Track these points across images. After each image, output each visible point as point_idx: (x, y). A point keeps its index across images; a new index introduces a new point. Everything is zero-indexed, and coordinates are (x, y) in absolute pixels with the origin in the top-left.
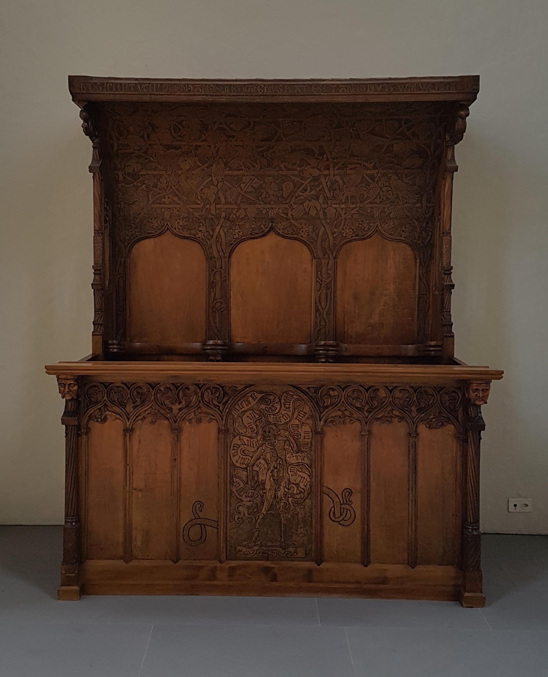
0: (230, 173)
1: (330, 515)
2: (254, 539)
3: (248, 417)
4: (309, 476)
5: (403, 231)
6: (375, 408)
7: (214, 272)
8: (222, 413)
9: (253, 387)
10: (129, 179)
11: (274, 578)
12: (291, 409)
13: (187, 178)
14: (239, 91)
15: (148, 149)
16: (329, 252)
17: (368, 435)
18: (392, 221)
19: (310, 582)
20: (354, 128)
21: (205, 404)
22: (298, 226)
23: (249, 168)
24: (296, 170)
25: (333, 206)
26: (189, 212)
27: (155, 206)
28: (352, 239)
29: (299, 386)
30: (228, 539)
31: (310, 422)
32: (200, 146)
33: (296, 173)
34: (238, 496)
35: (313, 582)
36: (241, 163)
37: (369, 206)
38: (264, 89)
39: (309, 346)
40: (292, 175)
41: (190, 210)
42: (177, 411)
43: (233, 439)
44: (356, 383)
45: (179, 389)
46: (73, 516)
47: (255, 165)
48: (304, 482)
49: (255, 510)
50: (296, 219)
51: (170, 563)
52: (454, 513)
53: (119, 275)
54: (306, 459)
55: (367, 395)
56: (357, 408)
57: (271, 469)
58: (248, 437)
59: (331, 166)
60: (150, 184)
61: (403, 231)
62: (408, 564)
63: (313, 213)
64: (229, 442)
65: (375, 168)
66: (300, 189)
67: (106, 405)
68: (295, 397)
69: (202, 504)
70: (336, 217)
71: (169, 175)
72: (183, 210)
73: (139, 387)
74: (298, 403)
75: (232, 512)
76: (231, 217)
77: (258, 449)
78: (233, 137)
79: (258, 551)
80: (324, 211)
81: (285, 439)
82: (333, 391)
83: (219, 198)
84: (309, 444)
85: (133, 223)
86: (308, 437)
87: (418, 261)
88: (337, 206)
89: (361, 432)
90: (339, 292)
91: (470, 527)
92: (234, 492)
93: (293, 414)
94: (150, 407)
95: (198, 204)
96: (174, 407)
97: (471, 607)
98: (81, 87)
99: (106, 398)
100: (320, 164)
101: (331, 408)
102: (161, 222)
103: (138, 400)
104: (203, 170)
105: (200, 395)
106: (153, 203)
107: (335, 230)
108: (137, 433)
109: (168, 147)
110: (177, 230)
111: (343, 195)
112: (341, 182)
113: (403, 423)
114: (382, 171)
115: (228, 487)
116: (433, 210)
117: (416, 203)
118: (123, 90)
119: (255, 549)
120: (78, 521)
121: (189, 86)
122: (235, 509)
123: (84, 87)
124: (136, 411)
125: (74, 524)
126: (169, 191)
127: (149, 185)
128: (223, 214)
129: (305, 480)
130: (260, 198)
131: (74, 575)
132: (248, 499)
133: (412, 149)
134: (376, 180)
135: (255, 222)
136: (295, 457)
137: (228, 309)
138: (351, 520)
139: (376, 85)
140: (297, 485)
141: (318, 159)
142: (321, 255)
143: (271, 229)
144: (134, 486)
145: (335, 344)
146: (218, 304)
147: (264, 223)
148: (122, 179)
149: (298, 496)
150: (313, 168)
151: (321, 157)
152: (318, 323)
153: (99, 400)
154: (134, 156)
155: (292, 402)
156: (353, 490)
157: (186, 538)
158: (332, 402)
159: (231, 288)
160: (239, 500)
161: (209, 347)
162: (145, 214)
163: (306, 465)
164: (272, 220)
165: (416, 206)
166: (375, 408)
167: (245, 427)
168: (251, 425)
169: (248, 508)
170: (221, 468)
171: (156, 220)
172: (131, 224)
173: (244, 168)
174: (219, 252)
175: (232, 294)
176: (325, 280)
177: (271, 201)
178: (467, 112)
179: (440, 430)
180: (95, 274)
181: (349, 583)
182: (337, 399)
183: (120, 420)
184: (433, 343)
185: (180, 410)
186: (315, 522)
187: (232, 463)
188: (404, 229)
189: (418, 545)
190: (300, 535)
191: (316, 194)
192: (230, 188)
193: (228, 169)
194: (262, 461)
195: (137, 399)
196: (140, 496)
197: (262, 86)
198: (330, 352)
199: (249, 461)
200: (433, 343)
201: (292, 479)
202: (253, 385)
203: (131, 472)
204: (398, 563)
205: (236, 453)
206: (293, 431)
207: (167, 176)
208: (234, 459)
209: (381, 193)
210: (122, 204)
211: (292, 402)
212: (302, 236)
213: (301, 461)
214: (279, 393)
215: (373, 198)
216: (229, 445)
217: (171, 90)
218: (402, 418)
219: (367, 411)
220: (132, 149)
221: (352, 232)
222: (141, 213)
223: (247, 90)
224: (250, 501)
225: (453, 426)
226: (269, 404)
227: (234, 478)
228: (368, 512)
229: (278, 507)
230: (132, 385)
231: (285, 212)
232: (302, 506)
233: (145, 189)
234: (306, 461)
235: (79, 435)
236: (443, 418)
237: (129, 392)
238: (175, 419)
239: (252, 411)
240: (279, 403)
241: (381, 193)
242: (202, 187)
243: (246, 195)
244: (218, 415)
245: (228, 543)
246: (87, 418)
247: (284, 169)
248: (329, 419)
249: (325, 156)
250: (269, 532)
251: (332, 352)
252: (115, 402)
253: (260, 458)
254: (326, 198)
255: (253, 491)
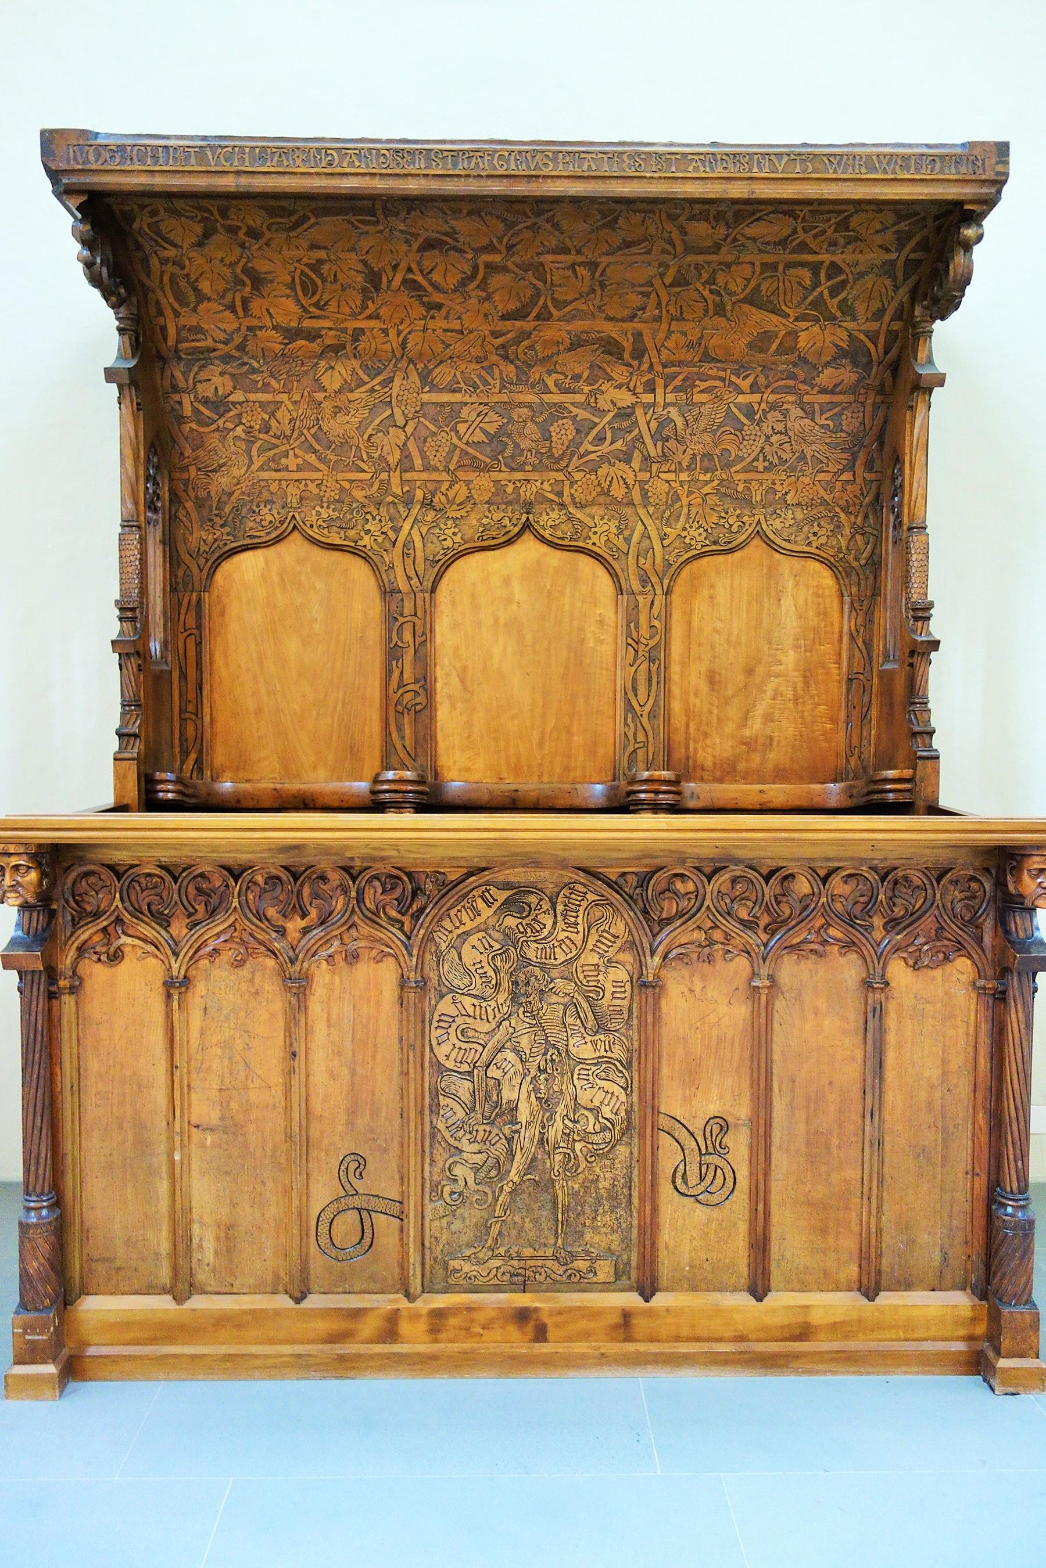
0: (434, 397)
1: (674, 1182)
2: (490, 1241)
3: (473, 947)
4: (625, 1089)
5: (815, 534)
6: (785, 922)
7: (398, 624)
8: (409, 938)
9: (486, 873)
10: (207, 412)
11: (541, 1334)
12: (580, 928)
13: (337, 410)
14: (450, 166)
15: (245, 339)
16: (654, 579)
17: (768, 987)
18: (790, 512)
19: (628, 1339)
20: (713, 287)
21: (367, 917)
22: (587, 520)
23: (476, 387)
24: (581, 392)
25: (663, 476)
26: (342, 489)
27: (265, 475)
28: (704, 550)
29: (600, 870)
30: (427, 1244)
31: (627, 957)
32: (362, 331)
33: (579, 398)
34: (452, 1141)
35: (636, 1341)
36: (458, 374)
37: (742, 476)
38: (508, 162)
39: (612, 788)
40: (572, 404)
41: (346, 485)
42: (297, 935)
43: (437, 1003)
44: (737, 861)
45: (302, 878)
46: (42, 1193)
47: (490, 379)
48: (612, 1105)
49: (493, 1173)
50: (581, 506)
51: (284, 1302)
52: (970, 1167)
53: (185, 630)
54: (616, 1048)
55: (767, 890)
56: (742, 922)
57: (533, 1073)
58: (475, 996)
59: (660, 383)
60: (253, 424)
61: (815, 534)
62: (859, 1290)
63: (618, 491)
64: (427, 1010)
65: (754, 388)
66: (590, 438)
67: (119, 921)
68: (591, 897)
69: (362, 1161)
70: (670, 502)
71: (295, 402)
72: (329, 485)
73: (202, 875)
74: (598, 912)
75: (436, 1177)
76: (436, 500)
77: (498, 1027)
78: (439, 307)
79: (502, 1270)
80: (642, 489)
81: (566, 999)
82: (683, 882)
83: (409, 457)
84: (626, 1011)
85: (216, 515)
86: (623, 996)
87: (847, 599)
88: (671, 476)
89: (751, 979)
90: (675, 668)
91: (1010, 1203)
92: (439, 1130)
93: (585, 940)
94: (230, 926)
95: (365, 471)
96: (290, 926)
97: (1013, 1394)
98: (72, 155)
99: (117, 902)
100: (634, 378)
101: (679, 922)
102: (278, 513)
103: (201, 908)
104: (372, 390)
105: (353, 894)
106: (261, 468)
107: (667, 530)
108: (200, 987)
109: (292, 334)
110: (315, 529)
111: (684, 452)
112: (680, 422)
113: (853, 956)
114: (772, 398)
115: (427, 1119)
116: (879, 488)
117: (842, 472)
118: (171, 162)
119: (491, 1266)
120: (58, 1203)
121: (329, 152)
122: (443, 1170)
123: (78, 154)
124: (195, 936)
125: (44, 1212)
126: (297, 439)
127: (251, 427)
128: (419, 495)
129: (614, 1098)
130: (500, 457)
131: (45, 1337)
132: (475, 1147)
133: (837, 346)
134: (757, 417)
135: (490, 511)
136: (589, 1044)
137: (430, 705)
138: (726, 1191)
139: (773, 157)
140: (596, 1111)
141: (630, 366)
142: (636, 586)
143: (527, 526)
144: (194, 1120)
145: (673, 778)
146: (408, 697)
147: (510, 514)
148: (189, 414)
149: (596, 1138)
150: (619, 387)
151: (637, 362)
152: (631, 738)
153: (102, 907)
154: (216, 358)
155: (582, 909)
156: (730, 1120)
157: (324, 1240)
158: (680, 908)
159: (438, 661)
160: (452, 1150)
161: (385, 787)
162: (243, 493)
163: (618, 1064)
164: (528, 507)
165: (842, 478)
166: (785, 922)
167: (468, 972)
168: (482, 967)
169: (477, 1169)
170: (407, 1073)
171: (269, 507)
172: (213, 517)
173: (465, 387)
174: (409, 578)
175: (439, 673)
176: (645, 642)
177: (525, 463)
178: (980, 231)
179: (938, 973)
180: (121, 619)
181: (720, 1340)
182: (693, 901)
183: (156, 957)
184: (891, 774)
185: (305, 931)
186: (640, 1198)
187: (434, 1059)
188: (816, 529)
189: (884, 1246)
190: (603, 1230)
191: (624, 449)
192: (434, 434)
193: (427, 389)
194: (510, 1056)
195: (197, 907)
196: (209, 1142)
197: (506, 154)
198: (661, 796)
199: (478, 1055)
200: (891, 774)
201: (584, 1098)
202: (484, 869)
203: (186, 1083)
204: (838, 1289)
205: (445, 1037)
206: (584, 982)
207: (291, 407)
208: (441, 1052)
209: (767, 447)
210: (193, 470)
211: (582, 909)
212: (594, 544)
213: (605, 1054)
214: (550, 888)
215: (749, 459)
216: (427, 1016)
217: (286, 163)
218: (849, 945)
219: (765, 929)
220: (210, 340)
221: (704, 534)
222: (233, 492)
223: (469, 163)
224: (480, 1152)
225: (969, 962)
226: (527, 916)
227: (441, 1098)
228: (767, 1174)
229: (548, 1164)
230: (184, 870)
231: (556, 489)
232: (608, 1163)
233: (243, 436)
234: (618, 1052)
235: (52, 996)
236: (946, 942)
237: (175, 887)
238: (291, 953)
239: (483, 934)
240: (551, 912)
241: (767, 447)
242: (370, 431)
243: (470, 450)
244: (399, 943)
245: (427, 1252)
246: (72, 953)
247: (553, 389)
248: (675, 952)
249: (646, 358)
250: (528, 1225)
251: (666, 796)
252: (142, 913)
253: (503, 1047)
254: (647, 458)
255: (488, 1128)
